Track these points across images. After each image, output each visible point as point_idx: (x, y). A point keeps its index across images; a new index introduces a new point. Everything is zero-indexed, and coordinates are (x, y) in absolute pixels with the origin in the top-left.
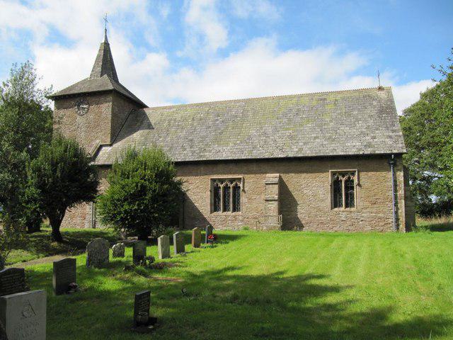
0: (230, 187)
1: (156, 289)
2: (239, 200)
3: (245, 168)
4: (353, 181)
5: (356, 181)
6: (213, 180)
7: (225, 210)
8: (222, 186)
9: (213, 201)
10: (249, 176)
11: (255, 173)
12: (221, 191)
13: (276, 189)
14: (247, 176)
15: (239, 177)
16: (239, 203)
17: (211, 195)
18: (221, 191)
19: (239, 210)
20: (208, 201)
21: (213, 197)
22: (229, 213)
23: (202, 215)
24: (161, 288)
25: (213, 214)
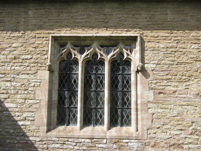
0: (76, 62)
1: (87, 22)
2: (126, 91)
3: (144, 14)
4: (128, 62)
5: (136, 62)
6: (59, 42)
7: (87, 121)
8: (81, 58)
9: (55, 97)
10: (155, 33)
11: (171, 27)
12: (79, 71)
13: (146, 61)
14: (149, 34)
15: (131, 34)
16: (126, 103)
17: (51, 82)
18: (79, 71)
19: (126, 122)
20: (42, 95)
21: (56, 86)
22: (100, 130)
23: (24, 135)
24: (82, 27)
25: (54, 133)
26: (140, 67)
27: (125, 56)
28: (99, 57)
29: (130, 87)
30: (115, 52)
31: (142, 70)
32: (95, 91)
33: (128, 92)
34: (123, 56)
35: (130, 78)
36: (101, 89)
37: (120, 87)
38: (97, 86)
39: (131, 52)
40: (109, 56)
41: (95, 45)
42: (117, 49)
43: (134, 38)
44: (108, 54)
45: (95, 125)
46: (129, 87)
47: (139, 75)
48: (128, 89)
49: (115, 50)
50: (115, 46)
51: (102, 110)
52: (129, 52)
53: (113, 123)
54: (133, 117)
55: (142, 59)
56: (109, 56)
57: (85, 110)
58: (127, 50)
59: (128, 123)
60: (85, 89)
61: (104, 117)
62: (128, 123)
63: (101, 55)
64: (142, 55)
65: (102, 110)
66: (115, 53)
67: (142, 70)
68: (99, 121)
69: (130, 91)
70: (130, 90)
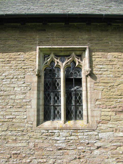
22: (60, 123)
26: (89, 71)
27: (77, 64)
28: (56, 64)
29: (81, 102)
30: (68, 61)
31: (91, 74)
32: (53, 106)
33: (80, 106)
34: (75, 64)
35: (81, 94)
36: (58, 104)
37: (73, 95)
38: (55, 101)
39: (81, 60)
40: (64, 64)
41: (53, 56)
42: (70, 58)
43: (84, 49)
44: (63, 62)
45: (54, 119)
46: (81, 102)
47: (89, 78)
48: (80, 104)
49: (68, 59)
50: (68, 56)
51: (59, 80)
52: (79, 60)
53: (68, 118)
54: (84, 113)
55: (91, 66)
56: (64, 64)
57: (45, 94)
58: (78, 59)
59: (81, 117)
60: (45, 90)
61: (60, 99)
62: (81, 117)
63: (58, 63)
64: (90, 60)
65: (59, 80)
66: (69, 61)
67: (91, 74)
68: (57, 116)
69: (82, 106)
70: (81, 104)
